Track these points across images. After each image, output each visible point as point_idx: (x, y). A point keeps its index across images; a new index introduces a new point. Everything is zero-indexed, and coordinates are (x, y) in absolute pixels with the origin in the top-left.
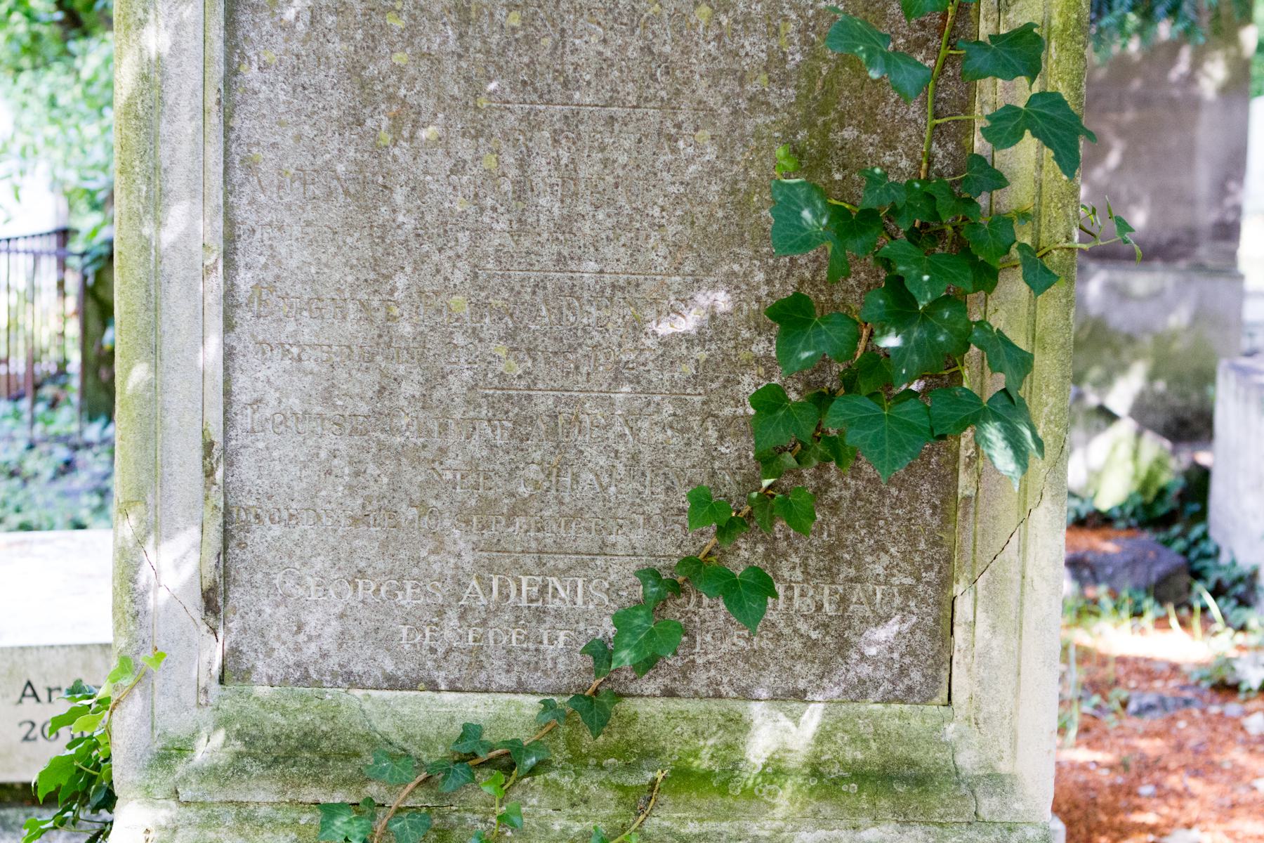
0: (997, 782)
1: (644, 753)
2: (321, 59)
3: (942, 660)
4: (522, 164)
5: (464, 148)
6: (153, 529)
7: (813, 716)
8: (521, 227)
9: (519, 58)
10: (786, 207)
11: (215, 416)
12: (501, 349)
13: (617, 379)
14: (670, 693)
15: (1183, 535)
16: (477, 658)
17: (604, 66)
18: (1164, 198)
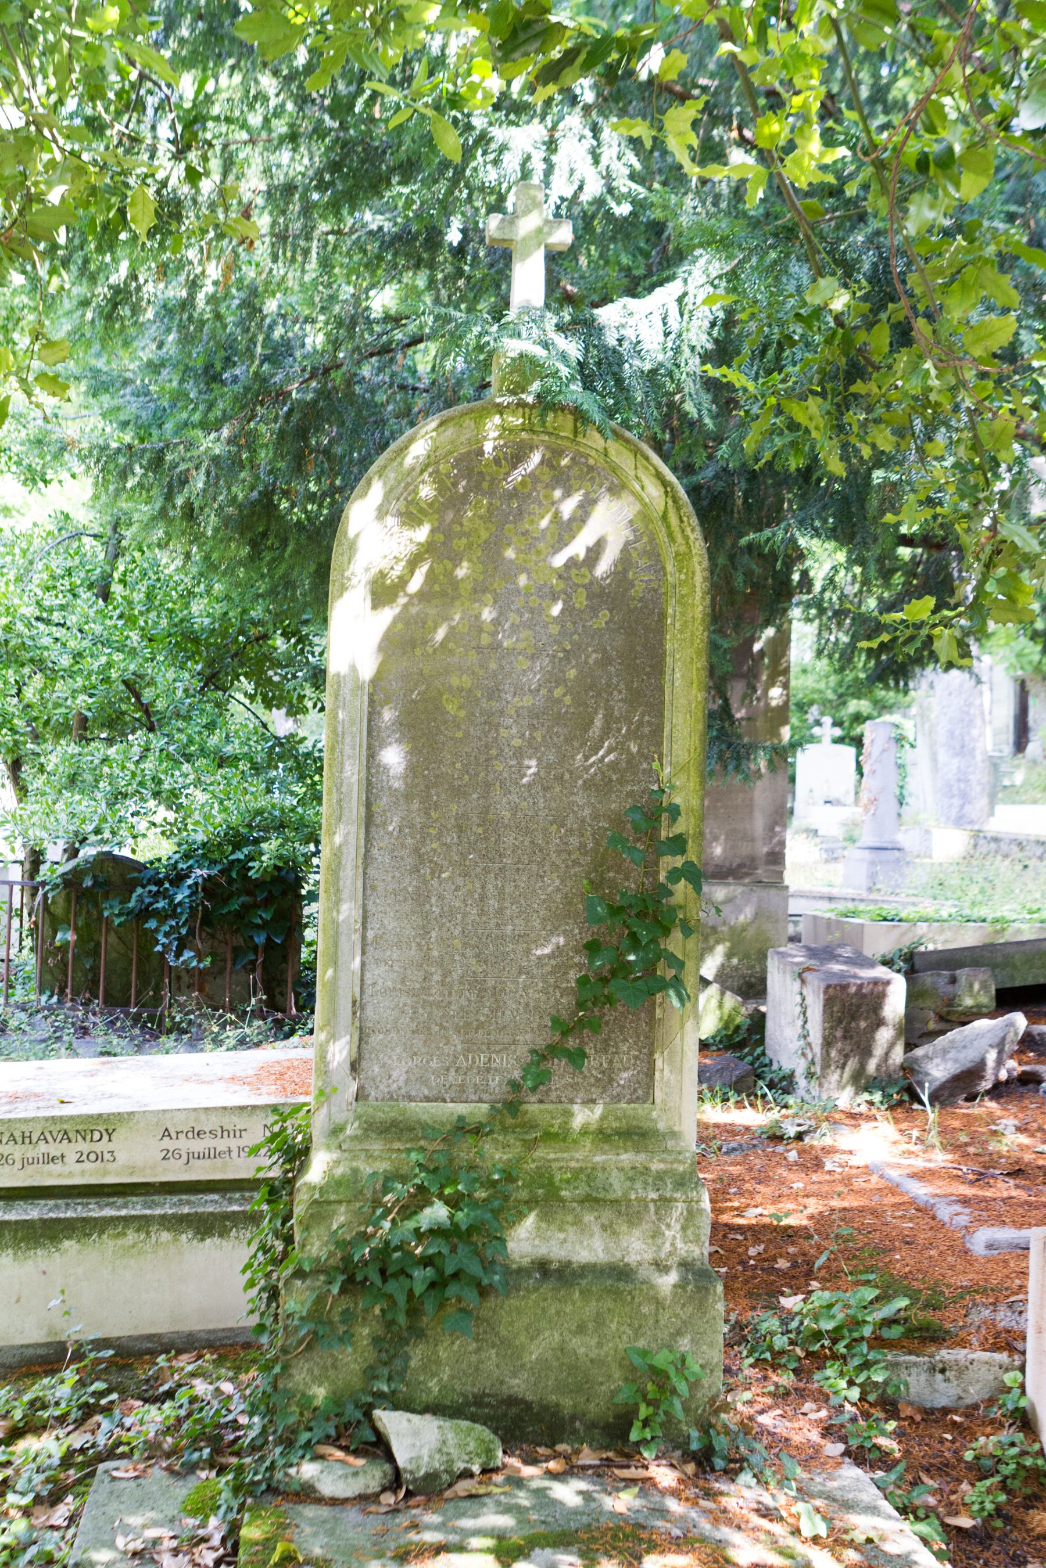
0: (674, 1135)
1: (532, 1126)
2: (403, 845)
3: (650, 1086)
4: (483, 887)
5: (459, 881)
6: (333, 1037)
7: (599, 1110)
8: (482, 912)
9: (481, 846)
10: (590, 907)
11: (357, 989)
12: (473, 961)
13: (520, 973)
14: (541, 1101)
15: (750, 1054)
16: (462, 1088)
17: (516, 848)
18: (736, 837)
